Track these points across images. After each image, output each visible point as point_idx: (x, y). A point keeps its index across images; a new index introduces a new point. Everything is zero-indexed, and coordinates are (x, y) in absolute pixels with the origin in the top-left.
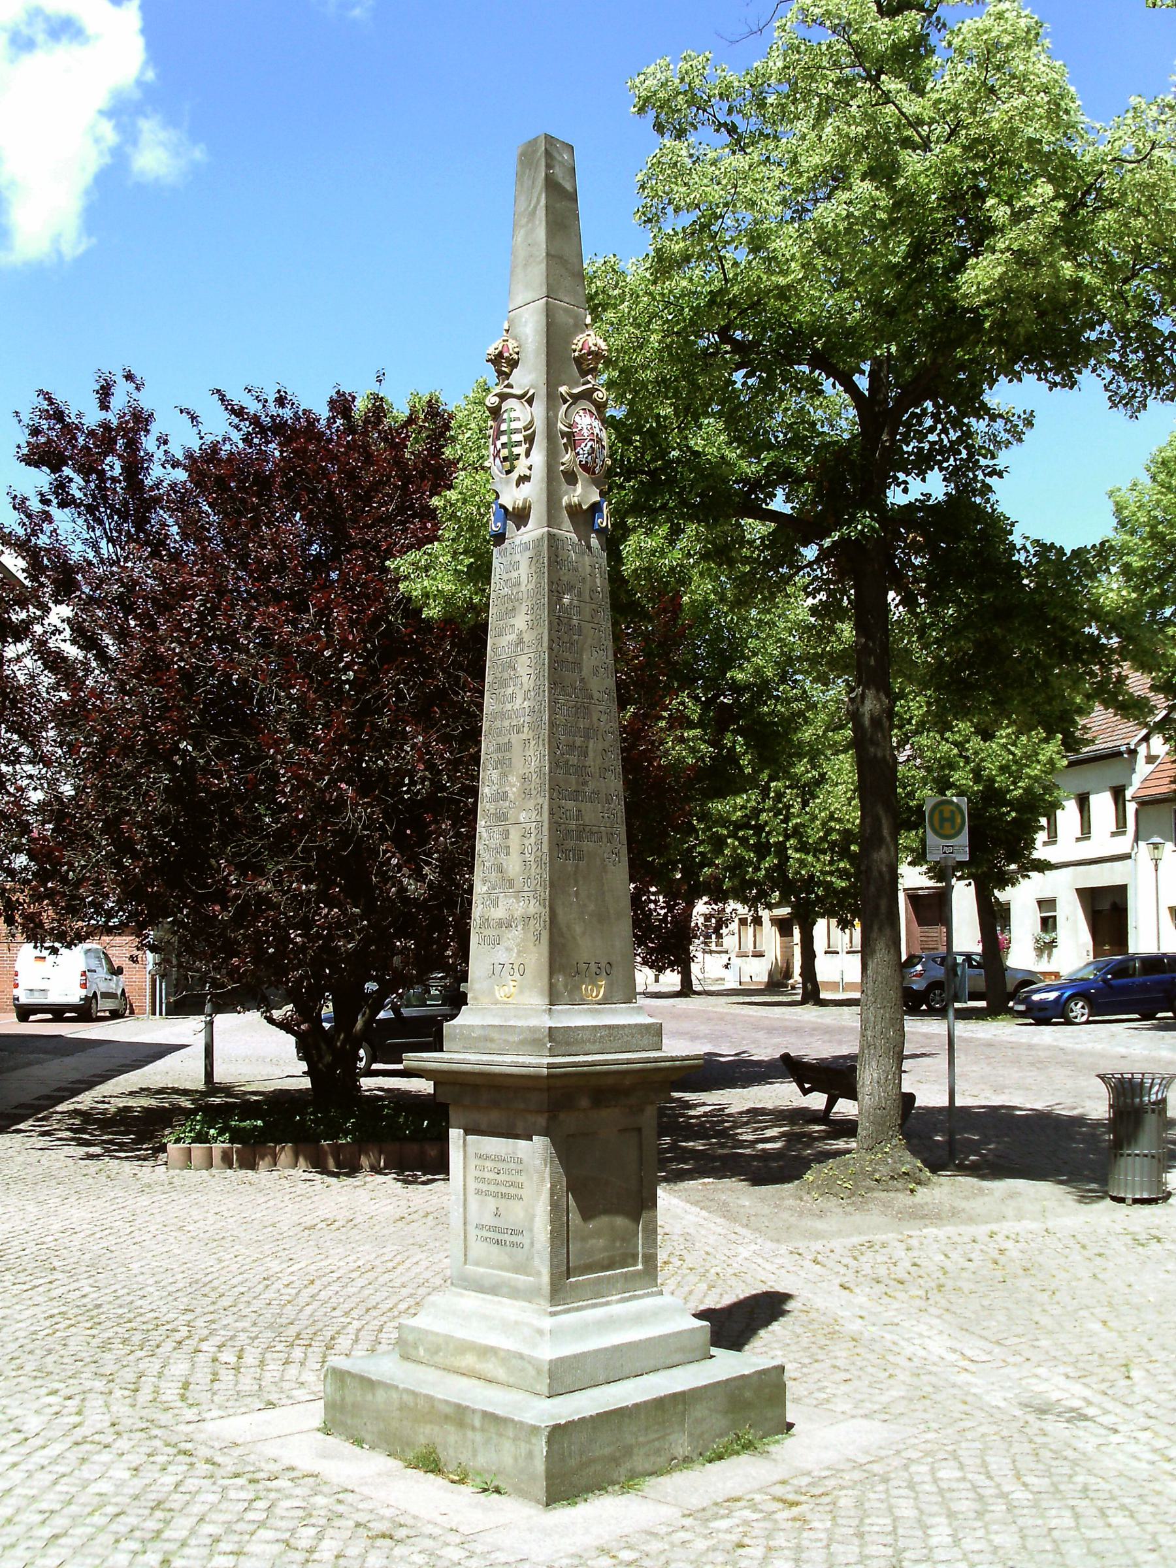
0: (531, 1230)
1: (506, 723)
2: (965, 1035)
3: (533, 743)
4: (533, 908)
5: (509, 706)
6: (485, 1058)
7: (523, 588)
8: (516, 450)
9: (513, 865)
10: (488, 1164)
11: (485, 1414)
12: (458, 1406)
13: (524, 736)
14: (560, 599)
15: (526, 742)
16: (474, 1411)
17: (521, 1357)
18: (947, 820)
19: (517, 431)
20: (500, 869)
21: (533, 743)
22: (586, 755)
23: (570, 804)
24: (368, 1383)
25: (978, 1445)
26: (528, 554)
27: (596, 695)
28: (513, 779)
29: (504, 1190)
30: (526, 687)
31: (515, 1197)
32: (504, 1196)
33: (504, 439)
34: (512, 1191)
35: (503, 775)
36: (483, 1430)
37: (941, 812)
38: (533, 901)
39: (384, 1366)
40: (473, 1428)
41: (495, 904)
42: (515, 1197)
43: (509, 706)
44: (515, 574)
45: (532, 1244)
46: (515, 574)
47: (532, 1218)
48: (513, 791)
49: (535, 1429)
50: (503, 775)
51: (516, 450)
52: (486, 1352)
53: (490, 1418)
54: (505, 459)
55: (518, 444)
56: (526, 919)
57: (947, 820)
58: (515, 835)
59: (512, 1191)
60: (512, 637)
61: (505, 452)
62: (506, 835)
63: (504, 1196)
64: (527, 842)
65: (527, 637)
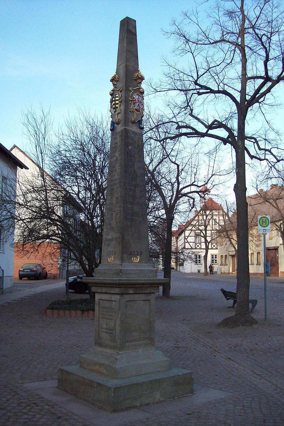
0: (115, 329)
1: (113, 183)
2: (252, 277)
3: (119, 188)
4: (118, 235)
5: (113, 178)
6: (103, 278)
7: (118, 144)
8: (117, 106)
9: (114, 223)
10: (105, 310)
11: (97, 383)
12: (91, 380)
13: (117, 186)
14: (128, 147)
15: (117, 188)
16: (94, 382)
17: (110, 366)
18: (264, 222)
19: (117, 100)
20: (110, 224)
21: (119, 188)
22: (135, 192)
23: (129, 206)
24: (69, 373)
25: (250, 399)
26: (120, 135)
27: (139, 175)
28: (114, 199)
29: (108, 317)
30: (118, 172)
31: (111, 319)
32: (109, 319)
33: (114, 103)
34: (111, 317)
35: (112, 198)
36: (97, 388)
37: (262, 220)
38: (118, 233)
39: (73, 369)
40: (94, 387)
41: (109, 235)
42: (111, 319)
43: (113, 178)
44: (116, 141)
45: (115, 333)
46: (116, 141)
47: (115, 325)
48: (114, 202)
49: (110, 388)
50: (112, 198)
51: (117, 106)
52: (101, 365)
53: (99, 384)
54: (114, 108)
55: (118, 104)
56: (116, 238)
57: (264, 222)
58: (114, 214)
59: (111, 317)
60: (115, 159)
61: (114, 106)
62: (112, 215)
63: (109, 319)
64: (117, 217)
65: (119, 158)
